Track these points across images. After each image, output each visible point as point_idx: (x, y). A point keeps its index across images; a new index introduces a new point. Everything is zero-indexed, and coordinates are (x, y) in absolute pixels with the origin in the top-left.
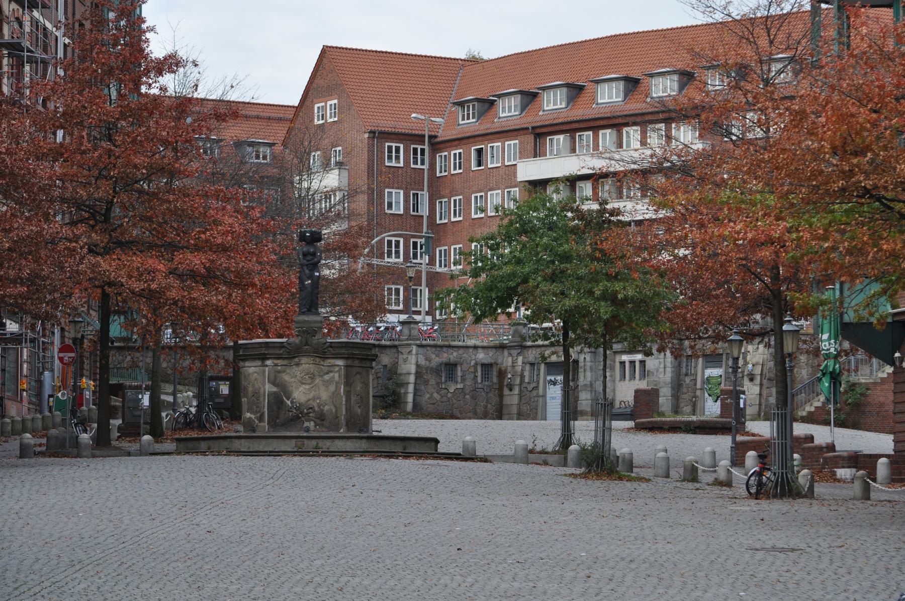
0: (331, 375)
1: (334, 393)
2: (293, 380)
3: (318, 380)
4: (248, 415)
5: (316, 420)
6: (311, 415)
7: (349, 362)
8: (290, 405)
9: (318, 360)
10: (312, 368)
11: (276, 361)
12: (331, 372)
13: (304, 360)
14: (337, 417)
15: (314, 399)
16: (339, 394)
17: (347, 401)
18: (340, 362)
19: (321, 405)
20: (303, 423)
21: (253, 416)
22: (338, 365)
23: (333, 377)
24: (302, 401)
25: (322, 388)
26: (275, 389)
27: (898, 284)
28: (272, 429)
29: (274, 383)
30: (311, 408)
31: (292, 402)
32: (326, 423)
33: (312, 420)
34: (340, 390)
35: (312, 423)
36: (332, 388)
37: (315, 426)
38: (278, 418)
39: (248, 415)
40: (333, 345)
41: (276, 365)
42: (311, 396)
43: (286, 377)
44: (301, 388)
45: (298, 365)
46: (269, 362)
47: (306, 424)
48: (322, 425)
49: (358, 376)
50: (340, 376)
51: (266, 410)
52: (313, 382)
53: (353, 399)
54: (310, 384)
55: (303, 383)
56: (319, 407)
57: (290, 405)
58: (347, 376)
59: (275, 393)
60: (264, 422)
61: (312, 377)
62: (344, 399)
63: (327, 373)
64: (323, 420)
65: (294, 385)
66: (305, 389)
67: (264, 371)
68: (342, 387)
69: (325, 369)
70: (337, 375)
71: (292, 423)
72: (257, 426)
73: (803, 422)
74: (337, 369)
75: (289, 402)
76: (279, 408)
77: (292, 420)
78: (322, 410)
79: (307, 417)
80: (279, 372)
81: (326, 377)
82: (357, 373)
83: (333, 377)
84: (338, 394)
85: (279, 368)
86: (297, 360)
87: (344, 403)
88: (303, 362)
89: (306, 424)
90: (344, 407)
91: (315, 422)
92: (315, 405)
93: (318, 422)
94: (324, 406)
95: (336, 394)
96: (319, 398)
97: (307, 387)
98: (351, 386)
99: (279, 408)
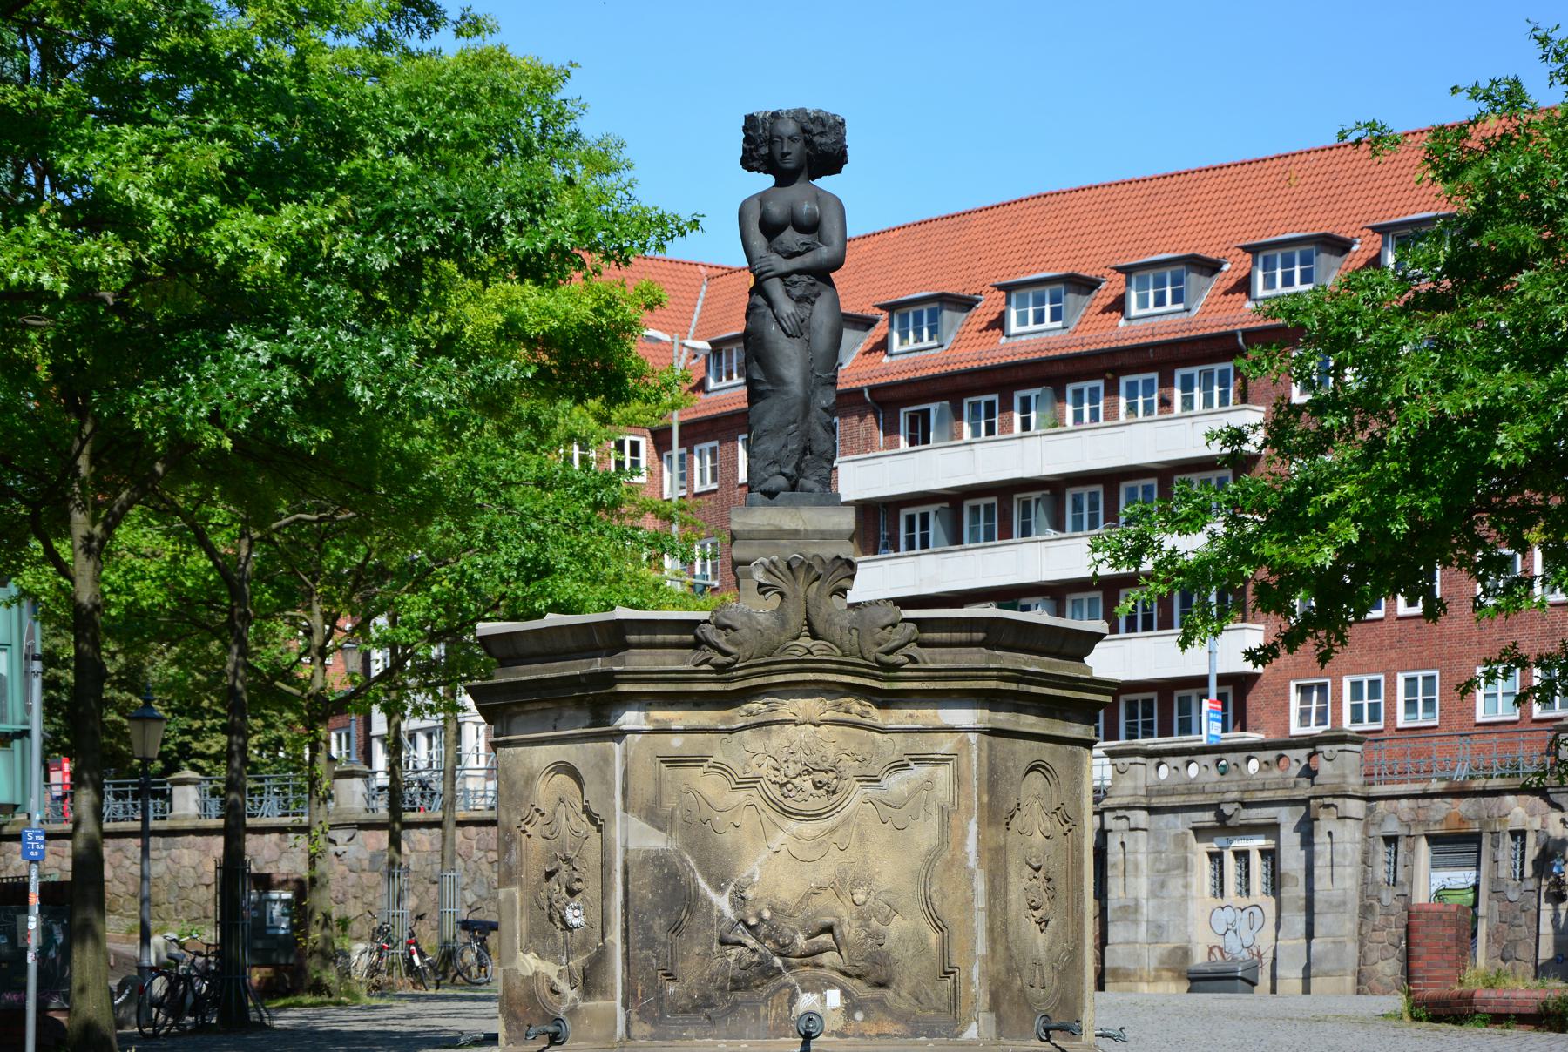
1: (931, 859)
4: (529, 963)
5: (853, 984)
6: (825, 958)
9: (855, 706)
15: (841, 885)
16: (956, 863)
19: (874, 913)
21: (549, 969)
23: (930, 782)
25: (880, 835)
26: (656, 841)
30: (829, 929)
31: (739, 900)
33: (832, 984)
34: (962, 844)
35: (834, 997)
36: (925, 834)
39: (529, 963)
42: (825, 871)
43: (707, 784)
46: (630, 719)
47: (807, 1001)
48: (881, 1003)
51: (616, 936)
56: (864, 921)
57: (729, 913)
58: (993, 780)
59: (658, 860)
60: (606, 992)
65: (745, 818)
67: (606, 760)
68: (973, 828)
69: (895, 747)
72: (572, 1012)
75: (722, 903)
77: (738, 984)
78: (877, 937)
80: (675, 762)
81: (896, 784)
83: (930, 782)
84: (949, 865)
91: (846, 994)
94: (887, 920)
95: (940, 859)
97: (808, 828)
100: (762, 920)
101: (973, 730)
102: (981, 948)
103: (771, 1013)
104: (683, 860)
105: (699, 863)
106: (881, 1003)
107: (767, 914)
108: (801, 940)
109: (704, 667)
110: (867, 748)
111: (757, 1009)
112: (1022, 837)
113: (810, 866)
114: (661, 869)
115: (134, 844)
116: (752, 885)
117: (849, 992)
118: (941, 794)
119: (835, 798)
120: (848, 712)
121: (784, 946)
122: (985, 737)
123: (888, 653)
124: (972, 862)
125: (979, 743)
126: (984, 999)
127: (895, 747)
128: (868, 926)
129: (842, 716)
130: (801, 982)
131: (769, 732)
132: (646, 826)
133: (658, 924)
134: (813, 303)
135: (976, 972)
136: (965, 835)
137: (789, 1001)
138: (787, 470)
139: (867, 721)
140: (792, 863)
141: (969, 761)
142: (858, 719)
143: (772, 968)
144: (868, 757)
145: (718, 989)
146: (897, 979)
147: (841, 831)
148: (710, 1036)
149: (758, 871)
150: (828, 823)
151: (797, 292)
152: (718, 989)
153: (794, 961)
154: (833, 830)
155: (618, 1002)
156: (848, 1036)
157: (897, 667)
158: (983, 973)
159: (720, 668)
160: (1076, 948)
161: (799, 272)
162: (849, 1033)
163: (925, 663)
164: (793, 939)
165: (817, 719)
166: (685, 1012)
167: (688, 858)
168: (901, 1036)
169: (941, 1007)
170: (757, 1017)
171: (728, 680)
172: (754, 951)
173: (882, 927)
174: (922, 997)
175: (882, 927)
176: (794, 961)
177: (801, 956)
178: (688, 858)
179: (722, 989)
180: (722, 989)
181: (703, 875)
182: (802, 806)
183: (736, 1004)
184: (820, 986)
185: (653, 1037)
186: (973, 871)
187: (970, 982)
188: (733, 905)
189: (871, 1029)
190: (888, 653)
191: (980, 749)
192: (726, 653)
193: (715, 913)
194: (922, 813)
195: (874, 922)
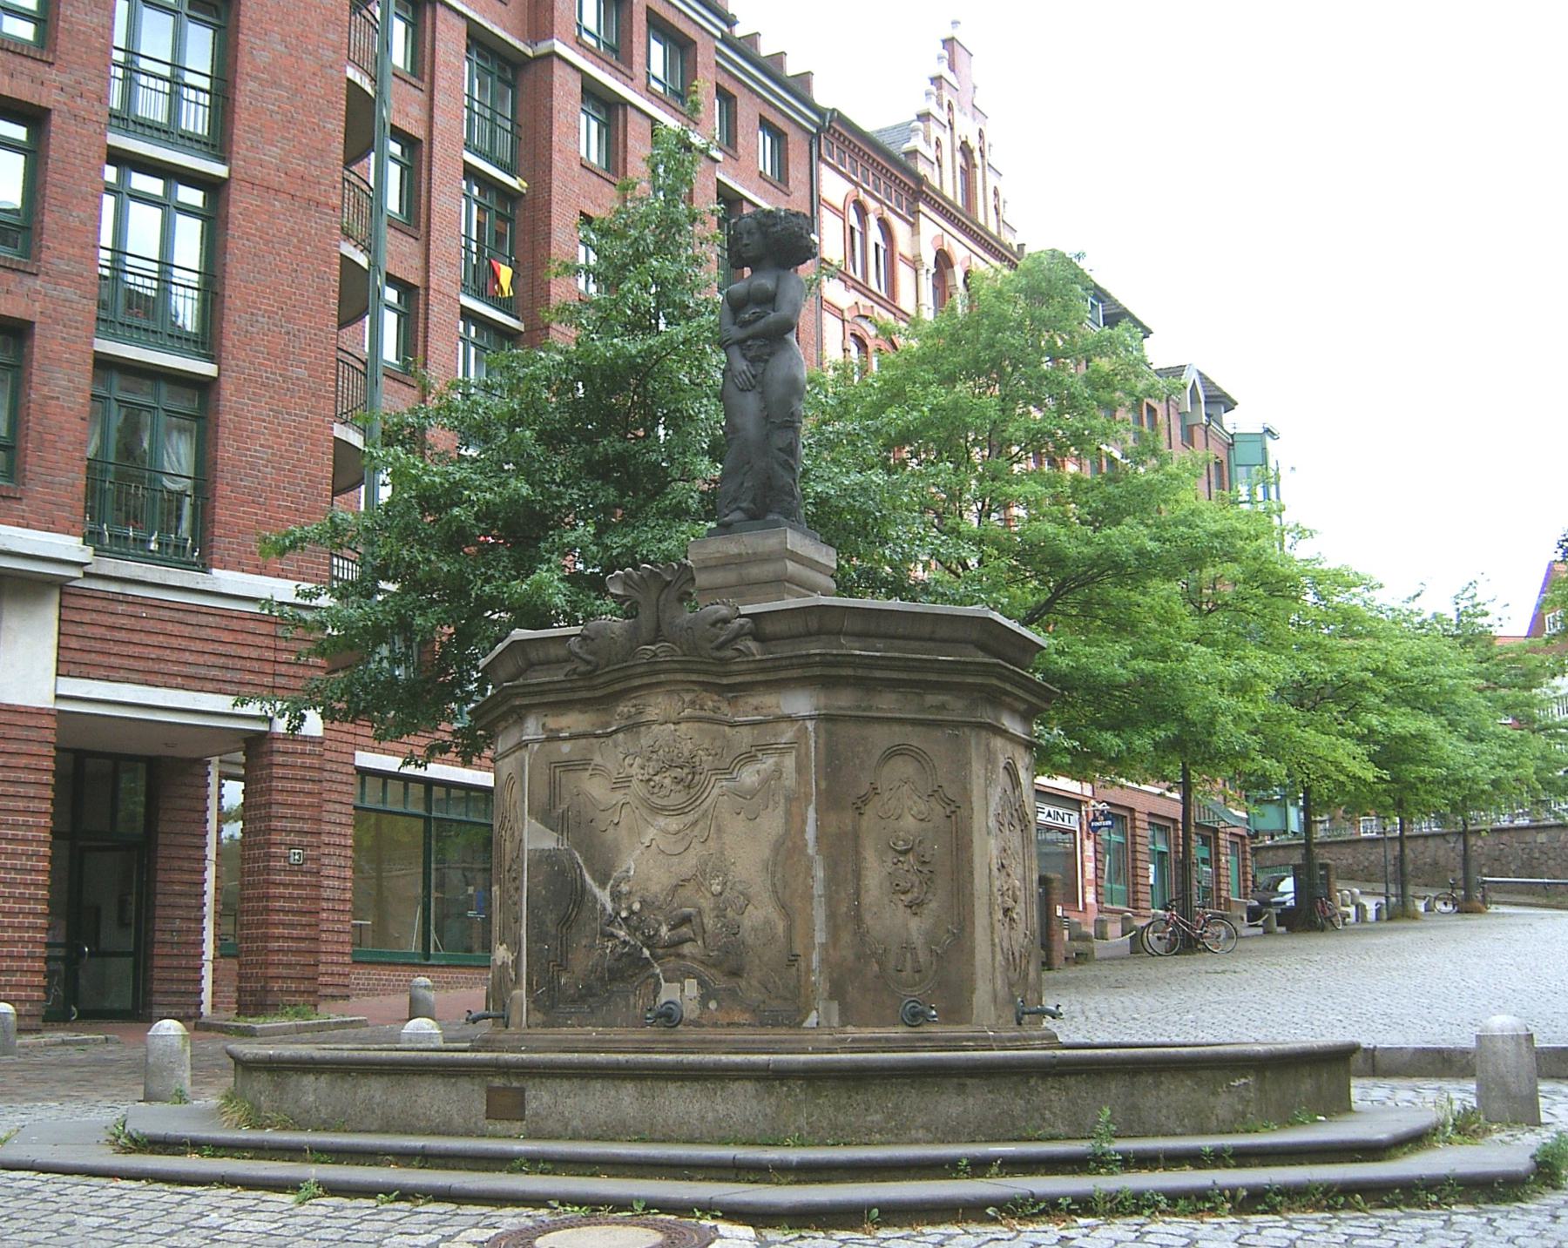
0: (769, 763)
2: (619, 797)
3: (716, 789)
5: (708, 973)
6: (687, 949)
7: (844, 700)
8: (609, 907)
10: (688, 740)
11: (552, 723)
12: (765, 748)
13: (658, 706)
14: (793, 959)
15: (698, 878)
16: (800, 848)
17: (832, 881)
18: (801, 703)
20: (658, 985)
22: (789, 719)
23: (778, 772)
24: (655, 888)
26: (549, 841)
27: (606, 435)
28: (539, 1017)
29: (549, 816)
30: (686, 920)
31: (616, 896)
32: (750, 987)
33: (689, 974)
34: (803, 831)
35: (691, 987)
36: (772, 823)
37: (704, 1000)
38: (563, 966)
40: (769, 628)
41: (553, 737)
42: (690, 862)
43: (596, 788)
44: (651, 833)
45: (633, 727)
48: (732, 993)
49: (903, 768)
50: (800, 769)
52: (693, 803)
53: (875, 873)
54: (679, 811)
55: (657, 810)
56: (721, 913)
57: (609, 907)
58: (834, 765)
61: (689, 775)
62: (820, 873)
63: (750, 758)
64: (735, 973)
65: (625, 817)
66: (665, 832)
68: (811, 814)
69: (744, 737)
70: (790, 762)
71: (617, 986)
73: (1534, 617)
74: (788, 733)
75: (604, 896)
76: (565, 922)
77: (615, 975)
78: (734, 930)
79: (672, 962)
80: (569, 766)
81: (749, 776)
82: (893, 753)
83: (778, 772)
85: (566, 748)
86: (624, 708)
87: (818, 889)
88: (652, 713)
89: (668, 993)
90: (819, 914)
91: (702, 984)
92: (706, 904)
93: (721, 983)
95: (786, 850)
96: (721, 870)
97: (674, 824)
98: (859, 807)
99: (565, 922)
100: (632, 913)
101: (811, 718)
102: (820, 937)
103: (639, 1002)
104: (572, 858)
105: (585, 861)
106: (732, 993)
107: (636, 907)
108: (664, 930)
109: (575, 677)
110: (718, 743)
111: (627, 999)
112: (883, 823)
113: (676, 860)
114: (553, 867)
115: (1472, 840)
116: (627, 879)
117: (704, 981)
118: (787, 783)
119: (692, 791)
120: (702, 708)
121: (650, 937)
122: (823, 725)
123: (720, 647)
124: (811, 850)
125: (816, 730)
126: (823, 987)
127: (744, 737)
128: (725, 917)
129: (702, 713)
130: (664, 972)
131: (638, 733)
132: (542, 827)
133: (550, 918)
134: (766, 361)
135: (815, 958)
136: (804, 822)
137: (654, 990)
138: (744, 505)
139: (718, 716)
140: (661, 857)
141: (808, 748)
142: (709, 714)
143: (640, 959)
144: (719, 751)
145: (598, 979)
146: (748, 967)
147: (701, 824)
148: (590, 1025)
149: (633, 866)
150: (691, 818)
151: (751, 354)
152: (598, 979)
153: (660, 951)
154: (695, 823)
155: (524, 992)
156: (703, 1026)
157: (724, 661)
158: (823, 961)
159: (586, 675)
160: (962, 929)
161: (754, 337)
162: (704, 1022)
163: (753, 655)
164: (657, 931)
165: (674, 717)
166: (574, 1001)
167: (577, 855)
168: (750, 1025)
169: (789, 996)
170: (627, 1006)
171: (594, 688)
172: (625, 943)
173: (737, 917)
174: (770, 986)
175: (737, 917)
176: (660, 951)
177: (664, 947)
178: (577, 855)
179: (602, 979)
180: (602, 979)
181: (588, 871)
182: (665, 802)
183: (612, 993)
184: (677, 976)
185: (545, 1025)
186: (813, 857)
187: (809, 970)
188: (613, 900)
189: (722, 1018)
190: (720, 647)
191: (817, 736)
192: (588, 663)
193: (599, 907)
194: (771, 803)
195: (730, 913)
